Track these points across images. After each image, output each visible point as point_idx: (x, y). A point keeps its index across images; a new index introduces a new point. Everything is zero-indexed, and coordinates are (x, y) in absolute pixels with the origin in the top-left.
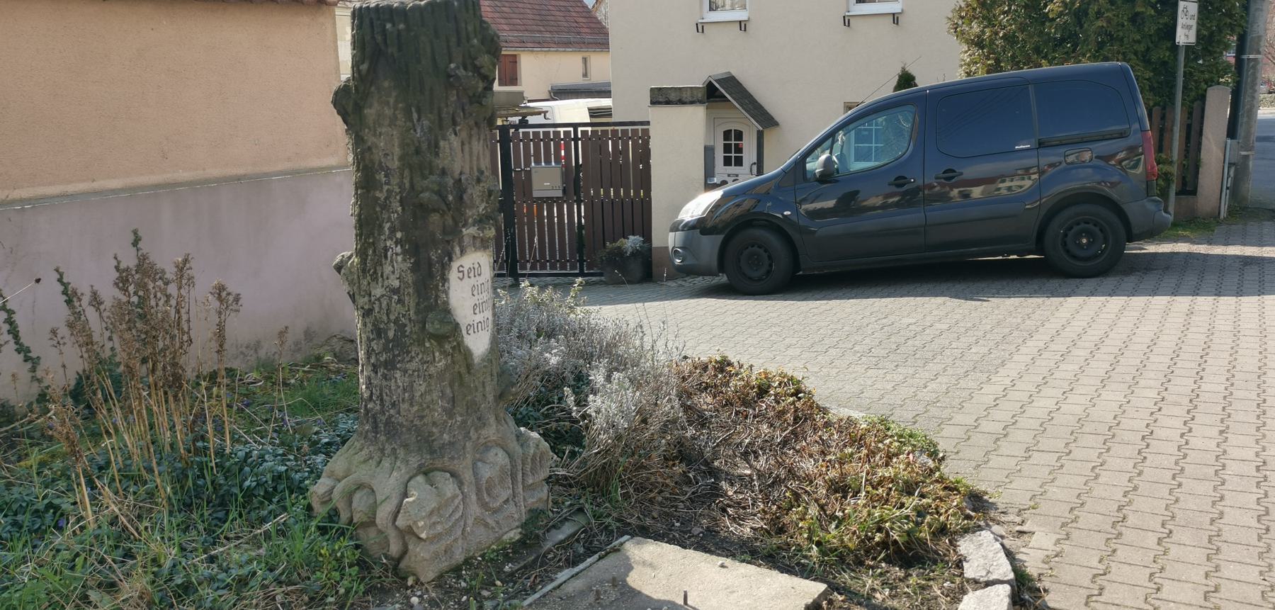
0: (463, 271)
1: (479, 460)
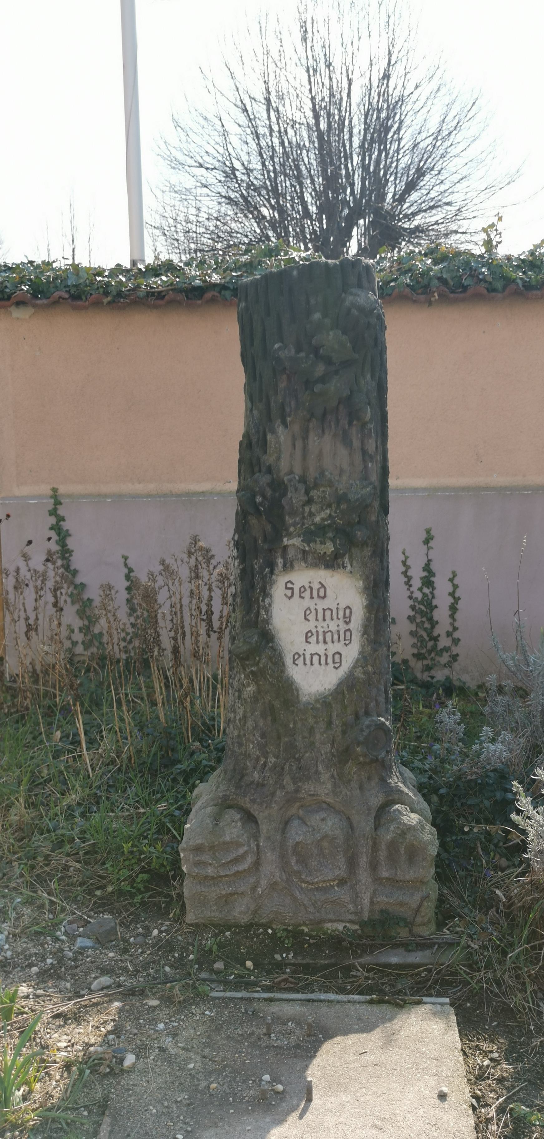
0: (292, 589)
1: (300, 818)
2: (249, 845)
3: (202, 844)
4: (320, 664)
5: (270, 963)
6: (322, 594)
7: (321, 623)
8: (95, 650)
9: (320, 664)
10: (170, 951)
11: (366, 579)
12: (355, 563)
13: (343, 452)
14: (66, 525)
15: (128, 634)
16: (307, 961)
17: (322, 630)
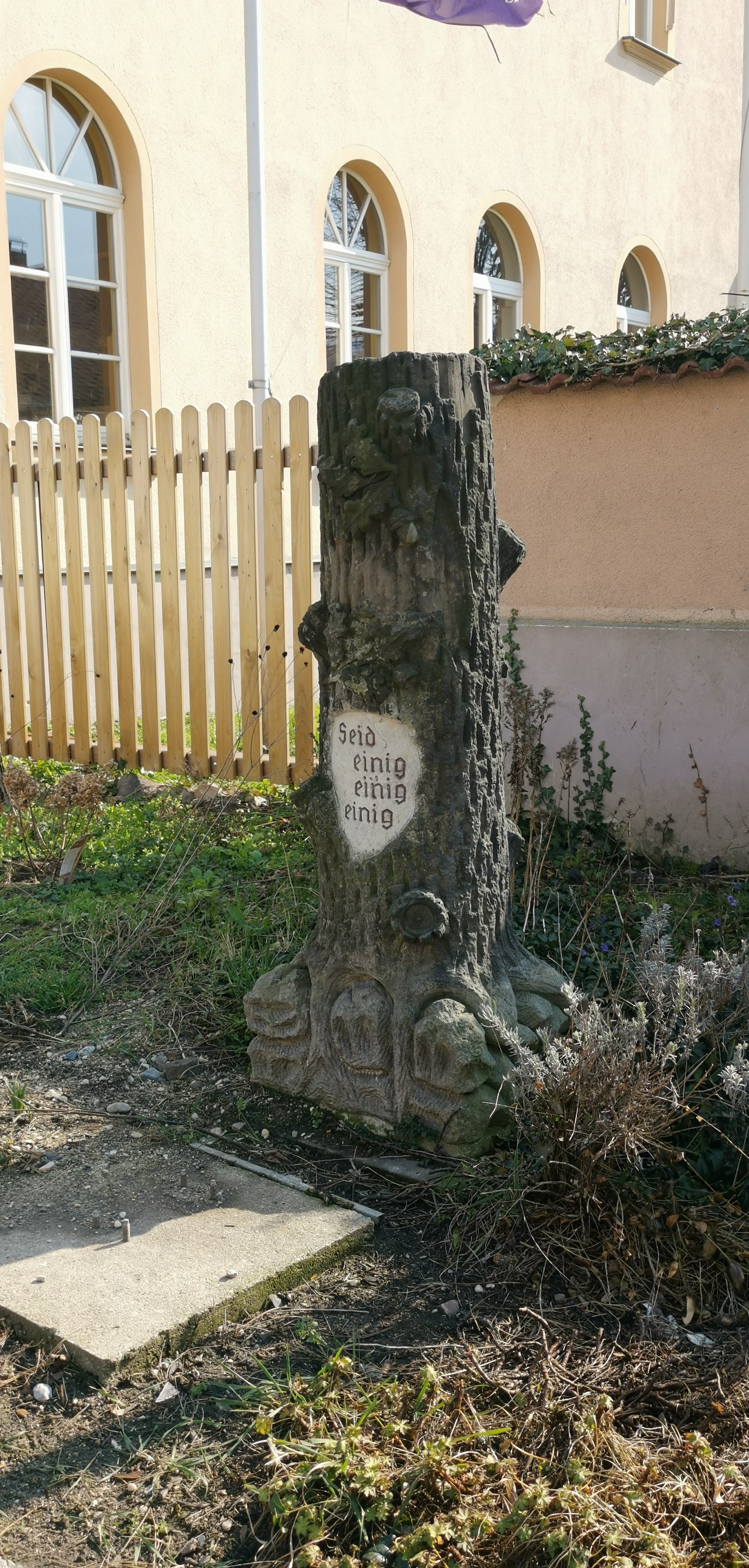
2: (299, 1011)
3: (260, 999)
4: (368, 821)
5: (285, 1138)
6: (371, 742)
7: (369, 774)
8: (544, 808)
9: (368, 821)
10: (211, 1101)
11: (421, 728)
12: (403, 708)
13: (383, 576)
14: (520, 655)
15: (581, 793)
16: (319, 1146)
17: (371, 782)
